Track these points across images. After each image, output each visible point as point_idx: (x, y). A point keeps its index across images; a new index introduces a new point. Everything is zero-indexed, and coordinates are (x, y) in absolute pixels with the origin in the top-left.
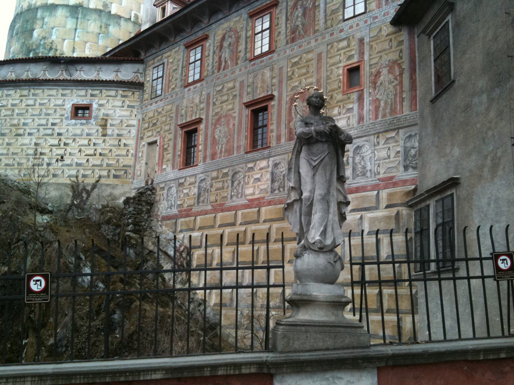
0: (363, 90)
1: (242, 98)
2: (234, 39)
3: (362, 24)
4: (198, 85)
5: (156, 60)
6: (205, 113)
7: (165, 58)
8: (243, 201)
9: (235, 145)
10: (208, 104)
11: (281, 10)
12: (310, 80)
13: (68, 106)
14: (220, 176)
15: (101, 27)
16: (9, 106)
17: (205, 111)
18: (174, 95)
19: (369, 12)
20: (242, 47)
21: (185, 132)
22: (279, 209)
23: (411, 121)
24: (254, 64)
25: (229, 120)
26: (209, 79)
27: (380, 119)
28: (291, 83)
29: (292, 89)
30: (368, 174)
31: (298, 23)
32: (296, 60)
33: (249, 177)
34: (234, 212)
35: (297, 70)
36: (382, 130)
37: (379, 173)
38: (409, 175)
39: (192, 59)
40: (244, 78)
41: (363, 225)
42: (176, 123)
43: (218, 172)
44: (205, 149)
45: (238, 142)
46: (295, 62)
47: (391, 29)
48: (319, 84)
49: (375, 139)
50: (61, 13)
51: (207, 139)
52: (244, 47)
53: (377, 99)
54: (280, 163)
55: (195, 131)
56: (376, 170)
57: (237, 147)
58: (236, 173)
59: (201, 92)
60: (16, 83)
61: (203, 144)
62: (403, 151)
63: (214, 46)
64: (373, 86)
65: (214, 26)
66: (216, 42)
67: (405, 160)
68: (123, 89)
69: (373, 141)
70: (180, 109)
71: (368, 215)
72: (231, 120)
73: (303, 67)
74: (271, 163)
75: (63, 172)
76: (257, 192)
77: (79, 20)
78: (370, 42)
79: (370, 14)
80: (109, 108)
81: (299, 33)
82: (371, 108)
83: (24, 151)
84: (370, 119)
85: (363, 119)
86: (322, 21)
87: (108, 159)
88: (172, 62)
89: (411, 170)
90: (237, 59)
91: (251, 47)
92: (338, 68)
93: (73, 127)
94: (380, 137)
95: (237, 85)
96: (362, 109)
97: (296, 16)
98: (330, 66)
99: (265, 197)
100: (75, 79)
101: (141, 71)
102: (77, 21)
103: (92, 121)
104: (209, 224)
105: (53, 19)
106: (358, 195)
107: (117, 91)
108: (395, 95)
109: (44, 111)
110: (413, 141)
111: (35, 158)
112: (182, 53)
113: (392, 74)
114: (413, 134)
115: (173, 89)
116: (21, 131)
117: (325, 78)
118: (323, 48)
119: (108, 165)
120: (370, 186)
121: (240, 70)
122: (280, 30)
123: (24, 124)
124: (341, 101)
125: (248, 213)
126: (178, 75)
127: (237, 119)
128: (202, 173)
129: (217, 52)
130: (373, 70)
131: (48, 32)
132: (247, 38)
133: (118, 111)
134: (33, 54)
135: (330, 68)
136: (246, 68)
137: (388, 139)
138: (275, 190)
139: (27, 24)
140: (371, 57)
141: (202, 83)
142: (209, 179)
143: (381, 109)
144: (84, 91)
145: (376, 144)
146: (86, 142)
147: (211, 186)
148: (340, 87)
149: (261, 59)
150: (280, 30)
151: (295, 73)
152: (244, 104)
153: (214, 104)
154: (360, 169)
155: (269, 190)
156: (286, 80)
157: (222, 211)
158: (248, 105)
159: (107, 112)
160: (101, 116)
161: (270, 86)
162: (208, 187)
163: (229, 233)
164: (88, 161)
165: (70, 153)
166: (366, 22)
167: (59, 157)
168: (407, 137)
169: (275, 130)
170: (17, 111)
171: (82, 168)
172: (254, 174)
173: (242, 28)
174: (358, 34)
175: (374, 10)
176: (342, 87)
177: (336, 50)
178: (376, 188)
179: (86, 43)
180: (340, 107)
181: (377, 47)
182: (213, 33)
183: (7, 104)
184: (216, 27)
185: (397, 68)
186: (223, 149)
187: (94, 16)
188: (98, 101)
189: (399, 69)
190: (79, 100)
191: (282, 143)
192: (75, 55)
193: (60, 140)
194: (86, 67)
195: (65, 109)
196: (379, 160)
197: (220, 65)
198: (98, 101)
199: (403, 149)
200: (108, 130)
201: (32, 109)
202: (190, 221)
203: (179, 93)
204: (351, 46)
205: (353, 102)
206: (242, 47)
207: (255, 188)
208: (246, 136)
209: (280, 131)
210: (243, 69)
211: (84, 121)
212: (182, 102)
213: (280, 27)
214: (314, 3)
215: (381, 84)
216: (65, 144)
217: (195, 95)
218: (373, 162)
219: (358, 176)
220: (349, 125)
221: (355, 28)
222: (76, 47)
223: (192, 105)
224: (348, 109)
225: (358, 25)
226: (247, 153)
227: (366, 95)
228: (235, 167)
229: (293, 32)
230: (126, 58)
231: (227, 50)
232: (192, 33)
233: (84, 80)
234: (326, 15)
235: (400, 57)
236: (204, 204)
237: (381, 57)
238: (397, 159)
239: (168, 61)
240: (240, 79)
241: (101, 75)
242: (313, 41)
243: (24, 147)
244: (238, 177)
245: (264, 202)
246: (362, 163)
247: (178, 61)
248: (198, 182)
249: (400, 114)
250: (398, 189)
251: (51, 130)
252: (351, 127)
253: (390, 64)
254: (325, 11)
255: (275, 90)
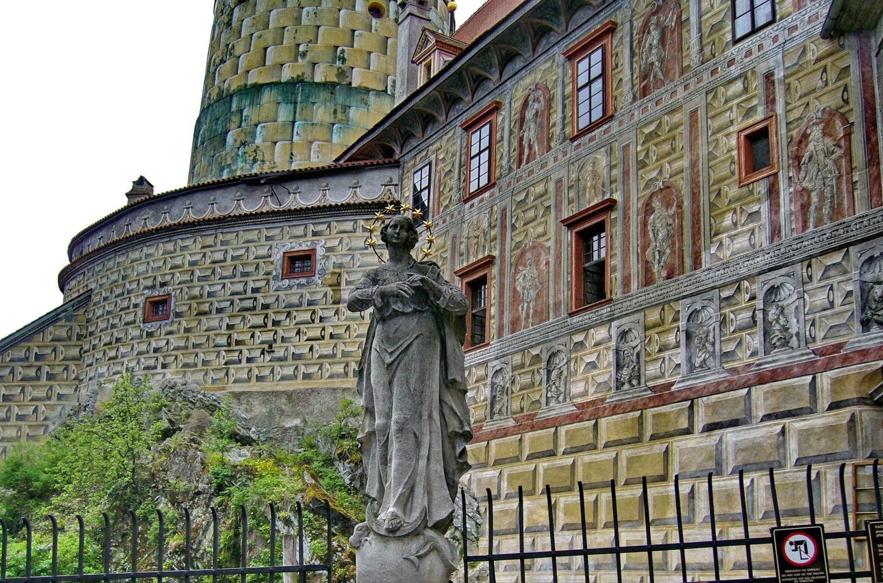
0: (776, 174)
1: (560, 210)
2: (542, 103)
3: (768, 45)
4: (487, 194)
5: (418, 159)
6: (498, 247)
7: (432, 154)
8: (569, 409)
9: (551, 303)
10: (503, 227)
11: (622, 37)
12: (677, 165)
13: (277, 257)
14: (528, 362)
15: (335, 112)
16: (186, 266)
17: (498, 241)
18: (448, 218)
19: (781, 19)
20: (557, 117)
21: (576, 233)
22: (632, 419)
23: (871, 228)
24: (579, 146)
25: (539, 255)
26: (503, 182)
27: (811, 229)
28: (645, 173)
29: (647, 186)
30: (794, 342)
31: (653, 58)
32: (652, 128)
33: (576, 362)
34: (553, 429)
35: (654, 148)
36: (816, 251)
37: (814, 339)
38: (871, 339)
39: (475, 151)
40: (563, 173)
41: (787, 446)
42: (452, 268)
43: (524, 354)
44: (501, 313)
45: (555, 296)
46: (650, 133)
47: (825, 47)
48: (695, 170)
49: (804, 271)
50: (267, 97)
51: (503, 293)
52: (560, 115)
53: (804, 189)
54: (630, 330)
55: (483, 280)
56: (808, 333)
57: (555, 304)
58: (553, 355)
59: (492, 207)
60: (195, 226)
61: (497, 304)
62: (859, 290)
63: (510, 121)
64: (796, 163)
65: (509, 84)
66: (513, 113)
67: (863, 309)
68: (366, 217)
69: (800, 273)
70: (458, 243)
71: (796, 425)
72: (543, 255)
73: (664, 141)
74: (614, 332)
75: (272, 372)
76: (592, 390)
77: (299, 105)
78: (785, 77)
79: (781, 24)
80: (344, 252)
81: (655, 77)
82: (793, 209)
83: (211, 341)
84: (792, 230)
85: (780, 231)
86: (695, 49)
87: (344, 343)
88: (444, 158)
89: (875, 329)
90: (549, 140)
91: (572, 115)
92: (727, 135)
93: (286, 292)
94: (814, 266)
95: (552, 186)
96: (777, 212)
97: (647, 45)
98: (713, 134)
99: (605, 399)
100: (287, 208)
101: (395, 182)
102: (295, 108)
103: (317, 279)
104: (511, 455)
105: (256, 109)
106: (776, 385)
107: (356, 221)
108: (839, 178)
109: (240, 268)
110: (877, 270)
111: (229, 351)
112: (459, 140)
113: (831, 136)
114: (877, 254)
115: (447, 206)
116: (206, 307)
117: (706, 157)
118: (699, 101)
119: (345, 354)
120: (799, 366)
121: (556, 159)
122: (620, 76)
123: (210, 294)
124: (738, 200)
125: (578, 430)
126: (453, 183)
127: (552, 252)
128: (497, 358)
129: (516, 130)
130: (794, 133)
131: (249, 133)
132: (564, 98)
133: (359, 256)
134: (228, 173)
135: (714, 137)
136: (565, 154)
137: (827, 268)
138: (623, 384)
139: (216, 124)
140: (789, 108)
141: (492, 190)
142: (509, 368)
143: (812, 208)
144: (302, 228)
145: (806, 279)
146: (307, 316)
147: (513, 382)
148: (733, 173)
149: (590, 135)
150: (620, 76)
151: (651, 154)
152: (563, 222)
153: (513, 226)
154: (777, 333)
155: (613, 384)
156: (635, 169)
157: (533, 428)
158: (570, 224)
159: (340, 261)
160: (331, 269)
161: (607, 182)
162: (508, 385)
163: (546, 470)
164: (311, 349)
165: (283, 337)
166: (775, 39)
167: (266, 346)
168: (866, 261)
169: (619, 267)
170: (198, 273)
171: (303, 362)
172: (584, 355)
173: (556, 80)
174: (762, 65)
175: (790, 14)
176: (737, 172)
177: (723, 100)
178: (810, 370)
179: (311, 142)
180: (735, 212)
181: (801, 87)
182: (508, 96)
183: (183, 264)
184: (513, 85)
185: (838, 123)
186: (531, 311)
187: (324, 95)
188: (325, 243)
189: (843, 125)
190: (294, 244)
191: (632, 292)
192: (294, 167)
193: (266, 317)
194: (304, 186)
195: (272, 263)
196: (812, 311)
197: (521, 154)
198: (325, 243)
199: (858, 287)
200: (342, 292)
201: (221, 267)
202: (479, 449)
203: (456, 213)
204: (750, 90)
205: (759, 200)
206: (557, 117)
207: (587, 382)
208: (568, 282)
209: (629, 268)
210: (560, 156)
211: (303, 281)
212: (461, 230)
213: (621, 71)
214: (679, 17)
215: (810, 158)
216: (276, 323)
217: (482, 215)
218: (802, 317)
219: (774, 346)
220: (753, 246)
221: (756, 54)
222: (294, 152)
223: (477, 233)
224: (750, 214)
225: (760, 47)
226: (571, 315)
227: (782, 184)
228: (553, 343)
229: (645, 77)
230: (368, 162)
231: (532, 126)
232: (475, 101)
233: (245, 214)
234: (701, 37)
235: (843, 100)
236: (502, 417)
237: (808, 104)
238: (847, 307)
239: (437, 158)
240: (555, 177)
241: (328, 197)
242: (680, 89)
243: (211, 333)
244: (558, 362)
245: (605, 408)
246: (782, 320)
247: (452, 156)
248: (490, 375)
249: (849, 215)
250: (852, 369)
251: (252, 301)
252: (757, 249)
253: (826, 116)
254: (700, 29)
255: (616, 191)
